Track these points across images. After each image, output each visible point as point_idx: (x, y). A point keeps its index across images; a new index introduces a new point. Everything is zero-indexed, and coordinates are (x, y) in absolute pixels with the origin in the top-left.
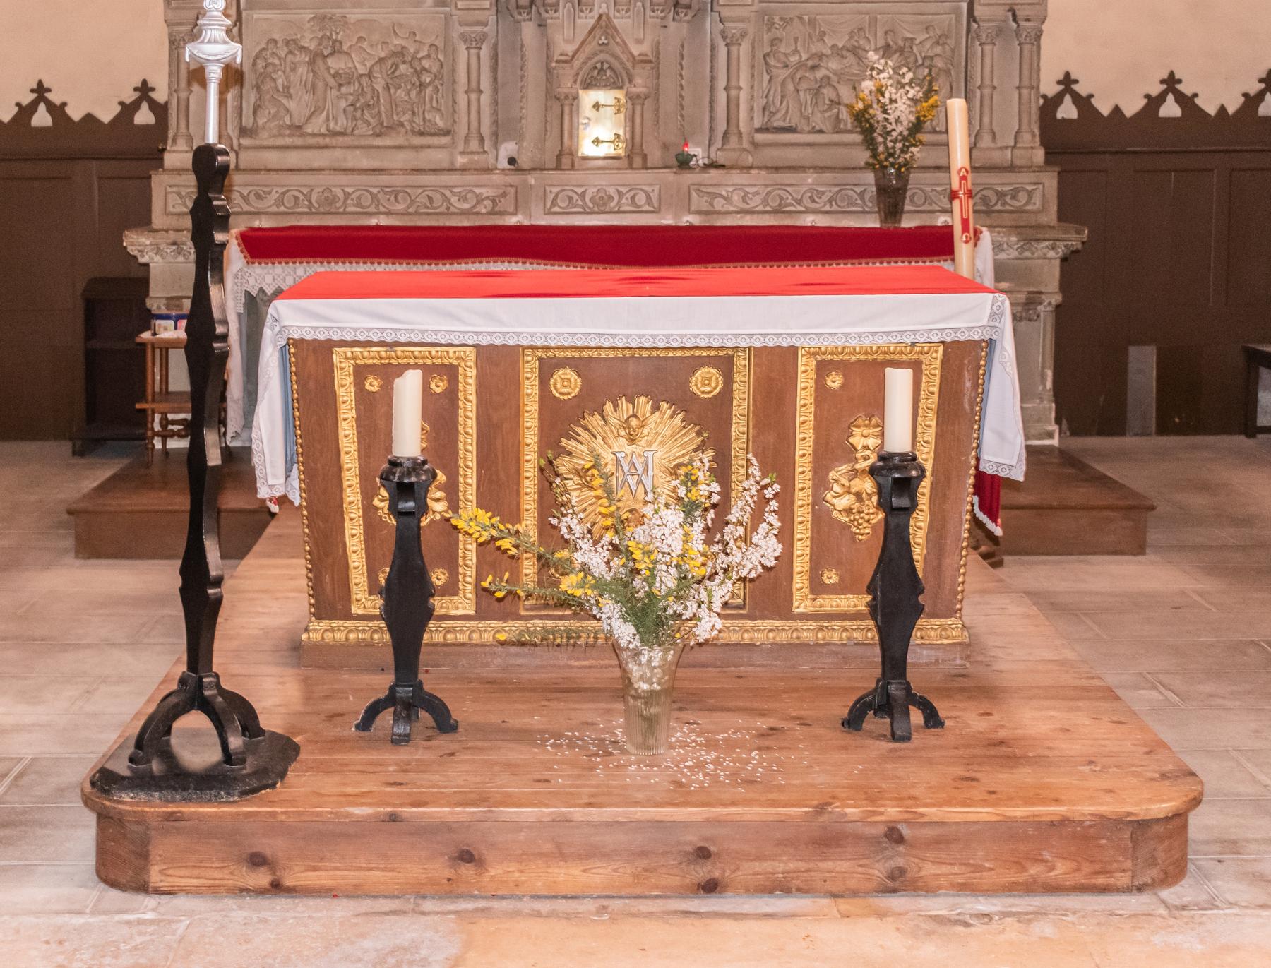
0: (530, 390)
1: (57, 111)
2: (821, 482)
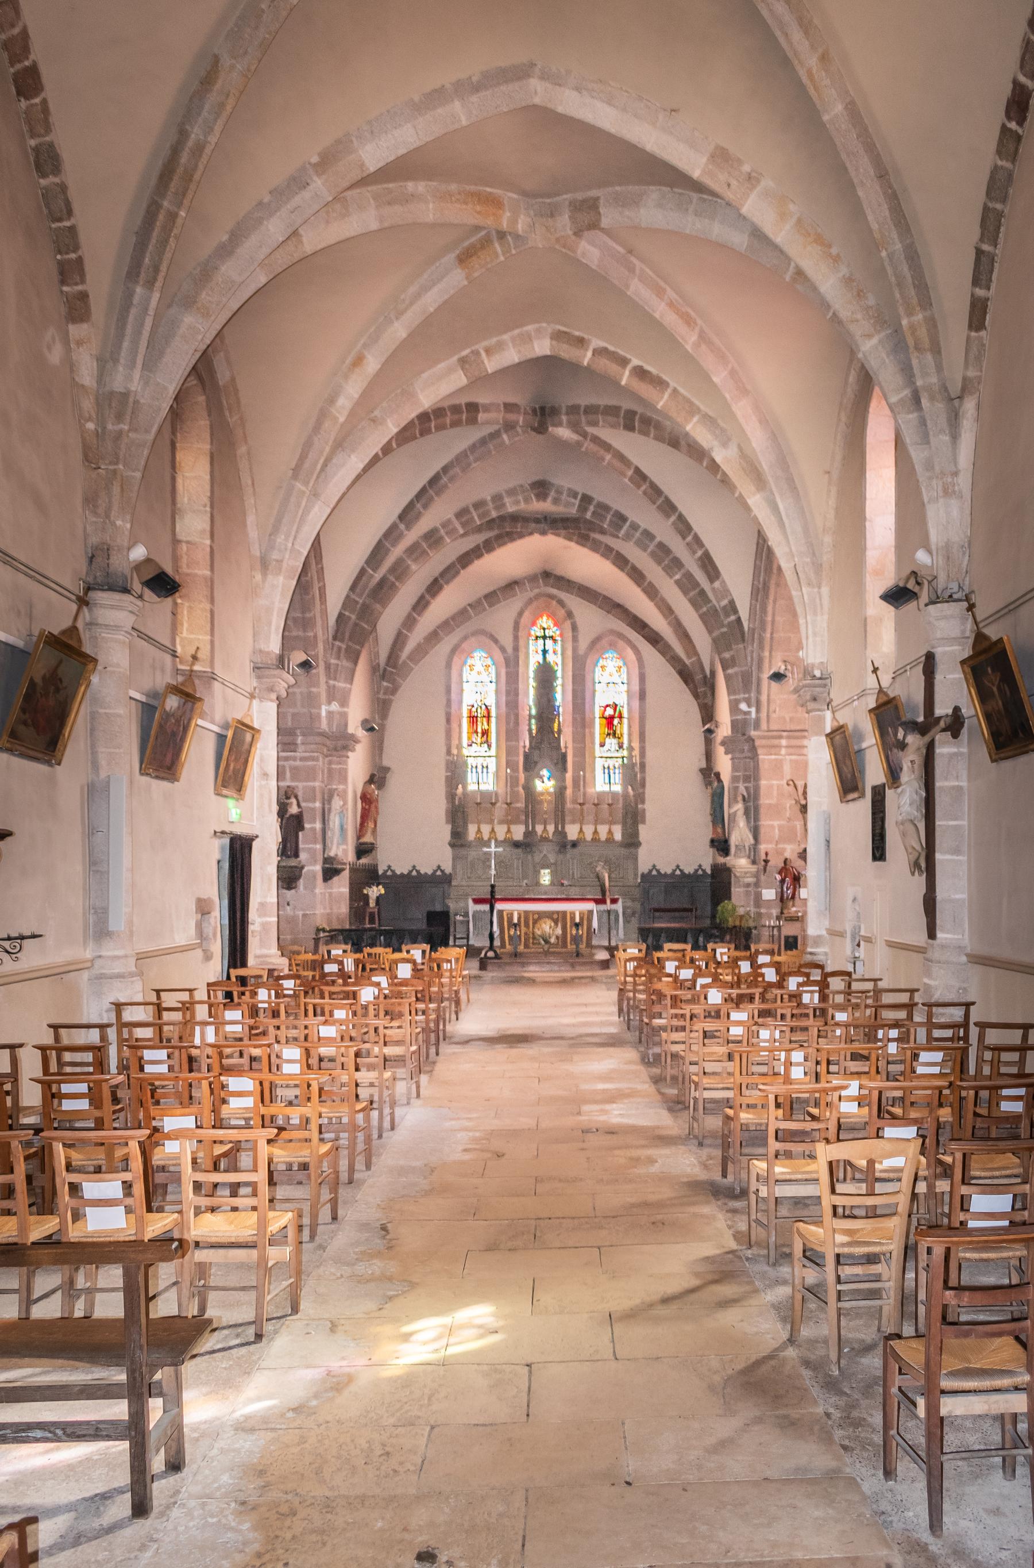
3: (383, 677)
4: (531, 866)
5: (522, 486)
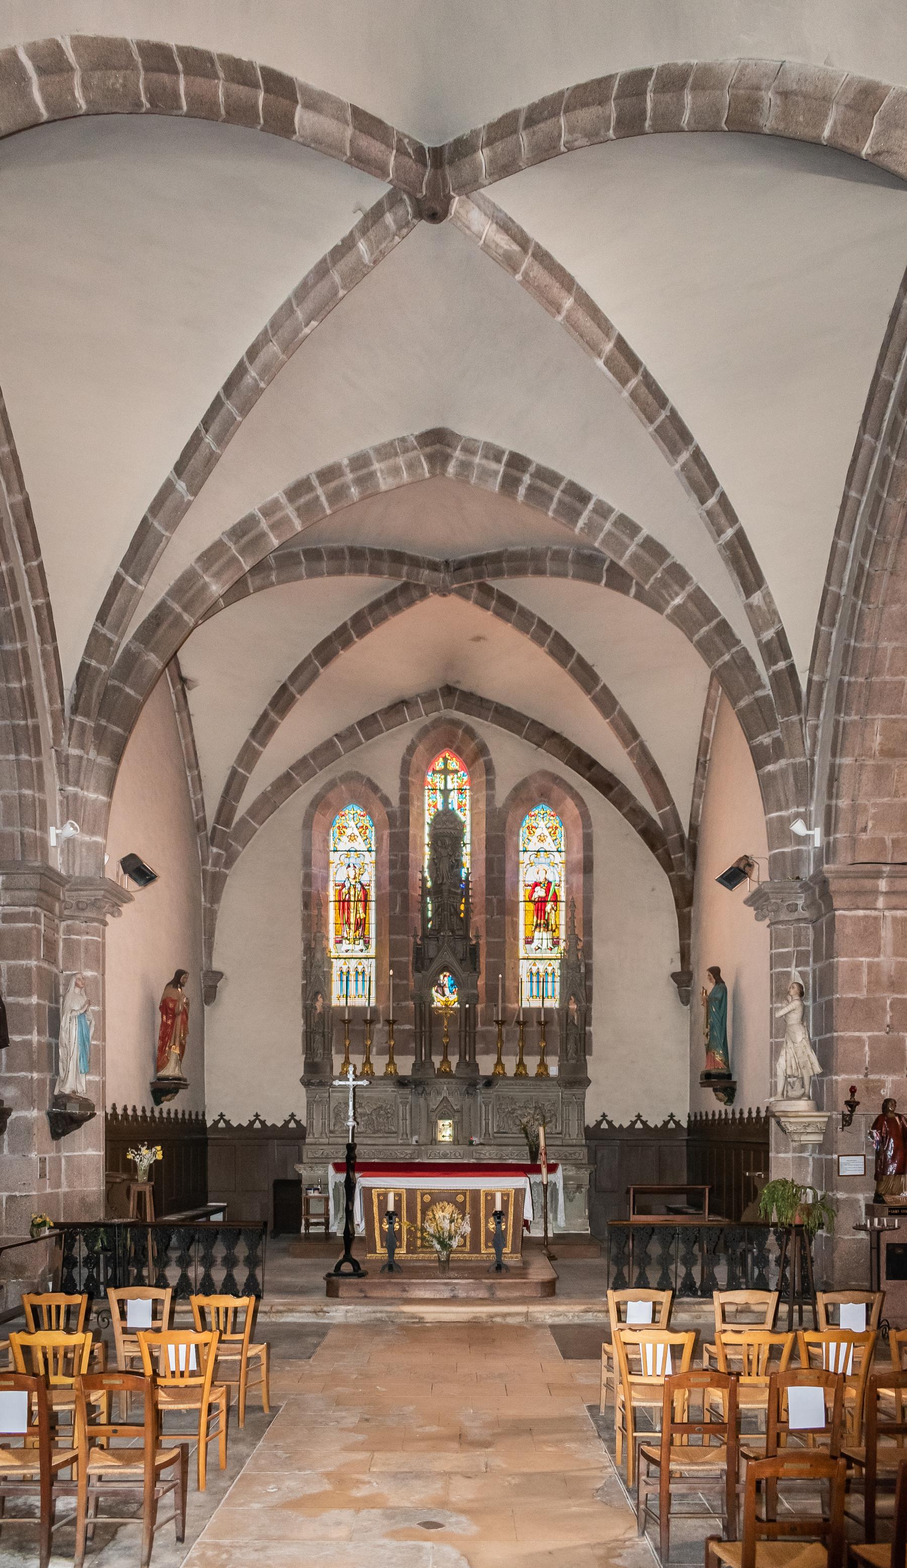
0: (419, 1200)
1: (263, 1123)
2: (487, 1222)
3: (212, 841)
4: (424, 1113)
5: (403, 440)
